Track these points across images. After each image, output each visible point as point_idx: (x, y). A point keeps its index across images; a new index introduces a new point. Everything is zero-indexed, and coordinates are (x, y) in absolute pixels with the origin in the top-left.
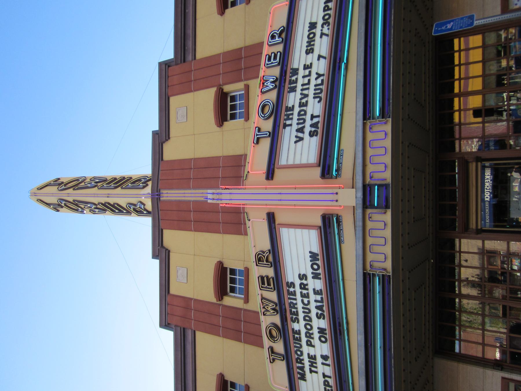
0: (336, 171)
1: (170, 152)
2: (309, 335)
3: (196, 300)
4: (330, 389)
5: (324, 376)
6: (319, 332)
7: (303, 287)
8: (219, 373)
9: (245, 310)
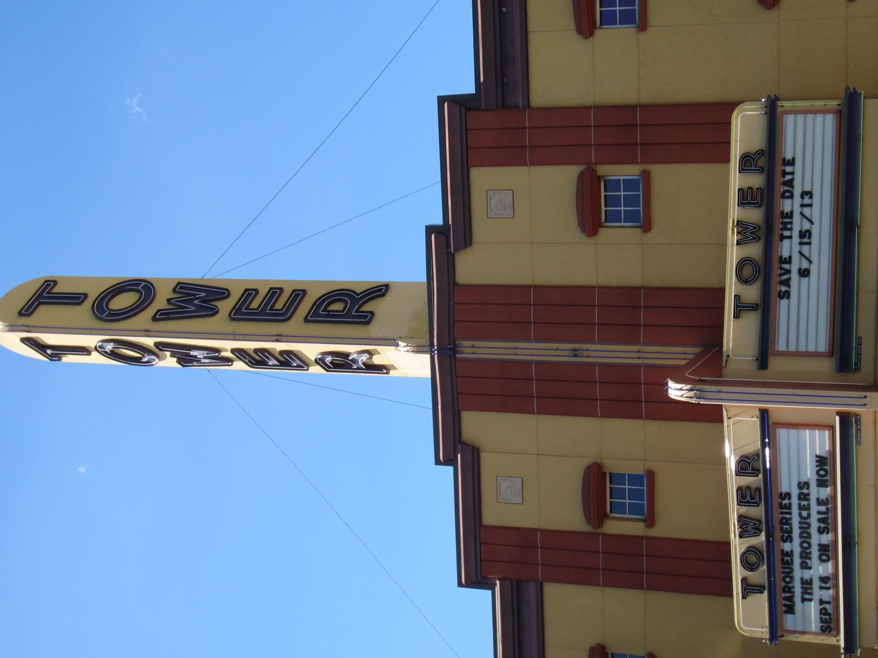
0: (856, 364)
1: (471, 268)
2: (805, 555)
3: (544, 532)
4: (827, 617)
5: (822, 602)
6: (819, 550)
7: (804, 497)
8: (592, 642)
9: (649, 538)
